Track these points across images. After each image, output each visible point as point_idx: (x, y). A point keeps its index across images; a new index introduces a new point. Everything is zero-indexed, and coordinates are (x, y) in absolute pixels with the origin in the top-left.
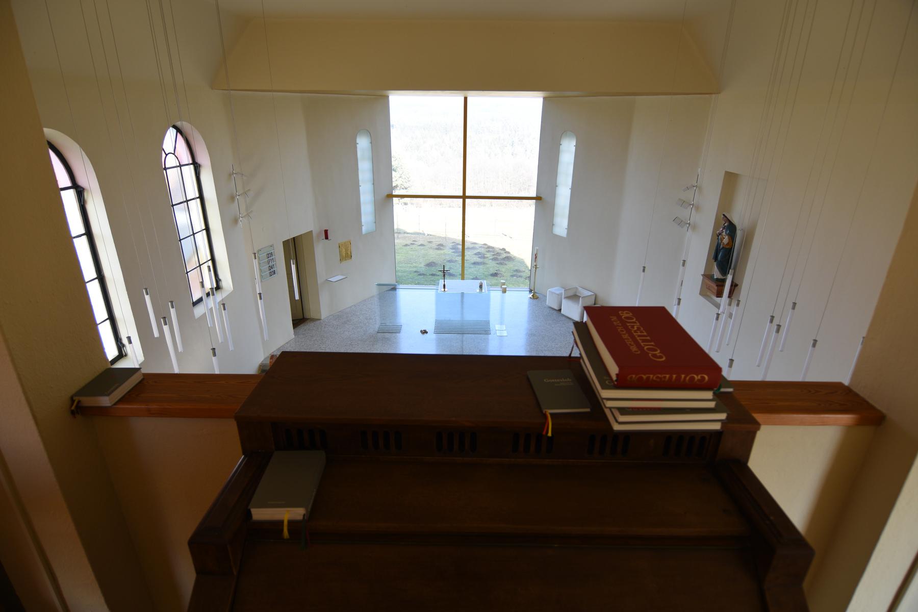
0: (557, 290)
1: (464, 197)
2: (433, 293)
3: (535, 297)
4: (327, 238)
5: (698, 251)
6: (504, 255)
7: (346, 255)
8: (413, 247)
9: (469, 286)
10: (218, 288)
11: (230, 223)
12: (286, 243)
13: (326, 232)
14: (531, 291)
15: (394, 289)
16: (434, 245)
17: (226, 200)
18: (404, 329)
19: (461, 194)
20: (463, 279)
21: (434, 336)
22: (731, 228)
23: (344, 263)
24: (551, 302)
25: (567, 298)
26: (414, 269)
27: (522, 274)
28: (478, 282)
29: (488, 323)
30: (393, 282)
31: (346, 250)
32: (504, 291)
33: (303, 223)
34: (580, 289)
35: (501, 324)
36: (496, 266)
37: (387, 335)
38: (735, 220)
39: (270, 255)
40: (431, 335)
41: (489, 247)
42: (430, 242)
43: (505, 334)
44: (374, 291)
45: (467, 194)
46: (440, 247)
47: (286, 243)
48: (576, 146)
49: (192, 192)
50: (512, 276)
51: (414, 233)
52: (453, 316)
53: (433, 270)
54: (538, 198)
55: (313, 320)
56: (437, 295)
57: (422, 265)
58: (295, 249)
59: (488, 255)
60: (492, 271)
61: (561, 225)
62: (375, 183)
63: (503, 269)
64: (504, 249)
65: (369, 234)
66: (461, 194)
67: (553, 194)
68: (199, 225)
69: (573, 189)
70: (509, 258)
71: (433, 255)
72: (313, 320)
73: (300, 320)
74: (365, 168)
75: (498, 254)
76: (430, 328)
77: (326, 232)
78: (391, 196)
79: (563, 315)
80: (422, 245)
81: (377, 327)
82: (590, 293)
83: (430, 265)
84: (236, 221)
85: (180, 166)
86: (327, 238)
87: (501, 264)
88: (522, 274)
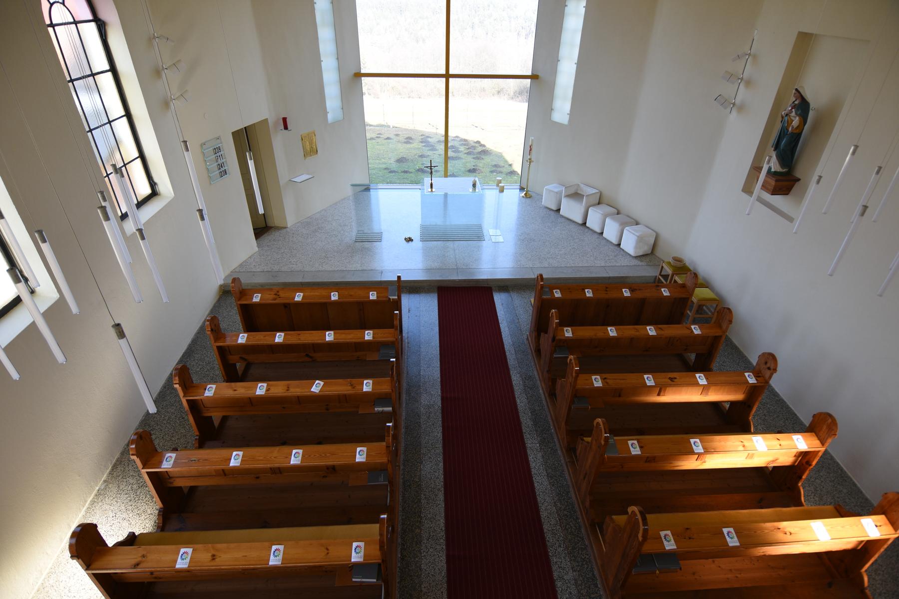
0: (554, 187)
1: (447, 76)
2: (418, 193)
3: (527, 196)
4: (286, 128)
5: (743, 137)
6: (480, 149)
7: (311, 151)
8: (379, 140)
9: (459, 186)
10: (154, 194)
11: (159, 107)
12: (236, 135)
13: (285, 120)
14: (522, 189)
15: (368, 189)
16: (401, 139)
17: (149, 75)
18: (385, 236)
19: (444, 72)
20: (446, 176)
21: (420, 244)
22: (803, 106)
23: (308, 158)
24: (548, 201)
25: (567, 196)
26: (384, 166)
27: (501, 169)
28: (470, 180)
29: (480, 227)
30: (366, 182)
31: (311, 143)
32: (502, 191)
33: (256, 109)
34: (582, 186)
35: (496, 227)
36: (478, 161)
37: (366, 245)
38: (809, 96)
39: (217, 150)
40: (417, 243)
41: (462, 140)
42: (397, 135)
43: (501, 239)
44: (349, 191)
45: (443, 71)
46: (409, 140)
47: (236, 135)
48: (586, 7)
49: (100, 62)
50: (492, 172)
51: (377, 126)
52: (436, 220)
53: (405, 166)
54: (534, 77)
55: (278, 228)
56: (423, 196)
57: (392, 161)
58: (247, 140)
59: (462, 149)
60: (470, 166)
61: (562, 109)
62: (339, 57)
63: (480, 164)
64: (478, 142)
65: (336, 123)
66: (444, 72)
67: (554, 72)
68: (117, 110)
69: (579, 64)
70: (485, 152)
71: (403, 150)
72: (278, 228)
73: (262, 228)
75: (474, 147)
76: (416, 235)
77: (285, 120)
78: (359, 75)
79: (562, 216)
80: (388, 138)
81: (354, 234)
82: (594, 191)
83: (401, 160)
84: (166, 104)
85: (76, 23)
86: (286, 128)
87: (478, 158)
88: (501, 169)
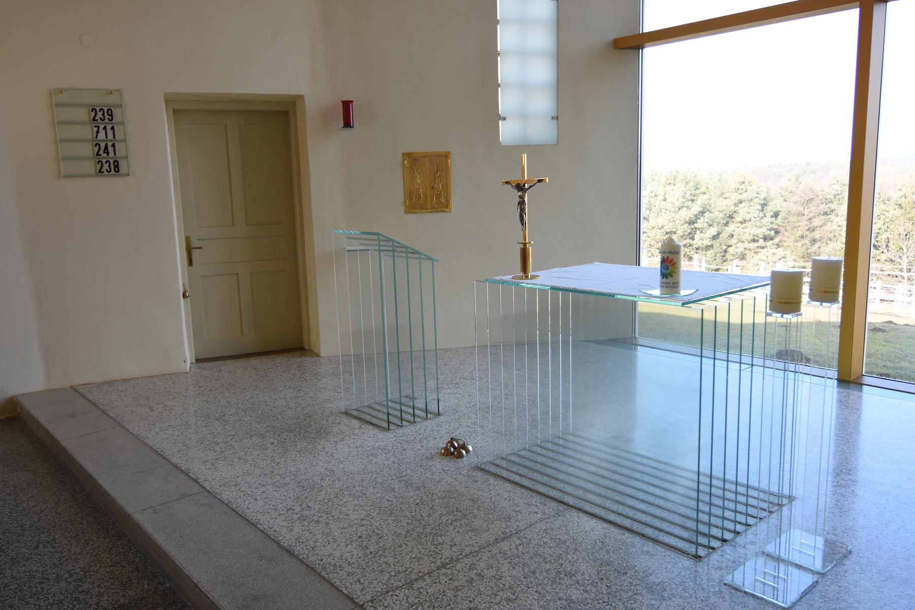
4: (347, 124)
13: (347, 105)
86: (347, 124)
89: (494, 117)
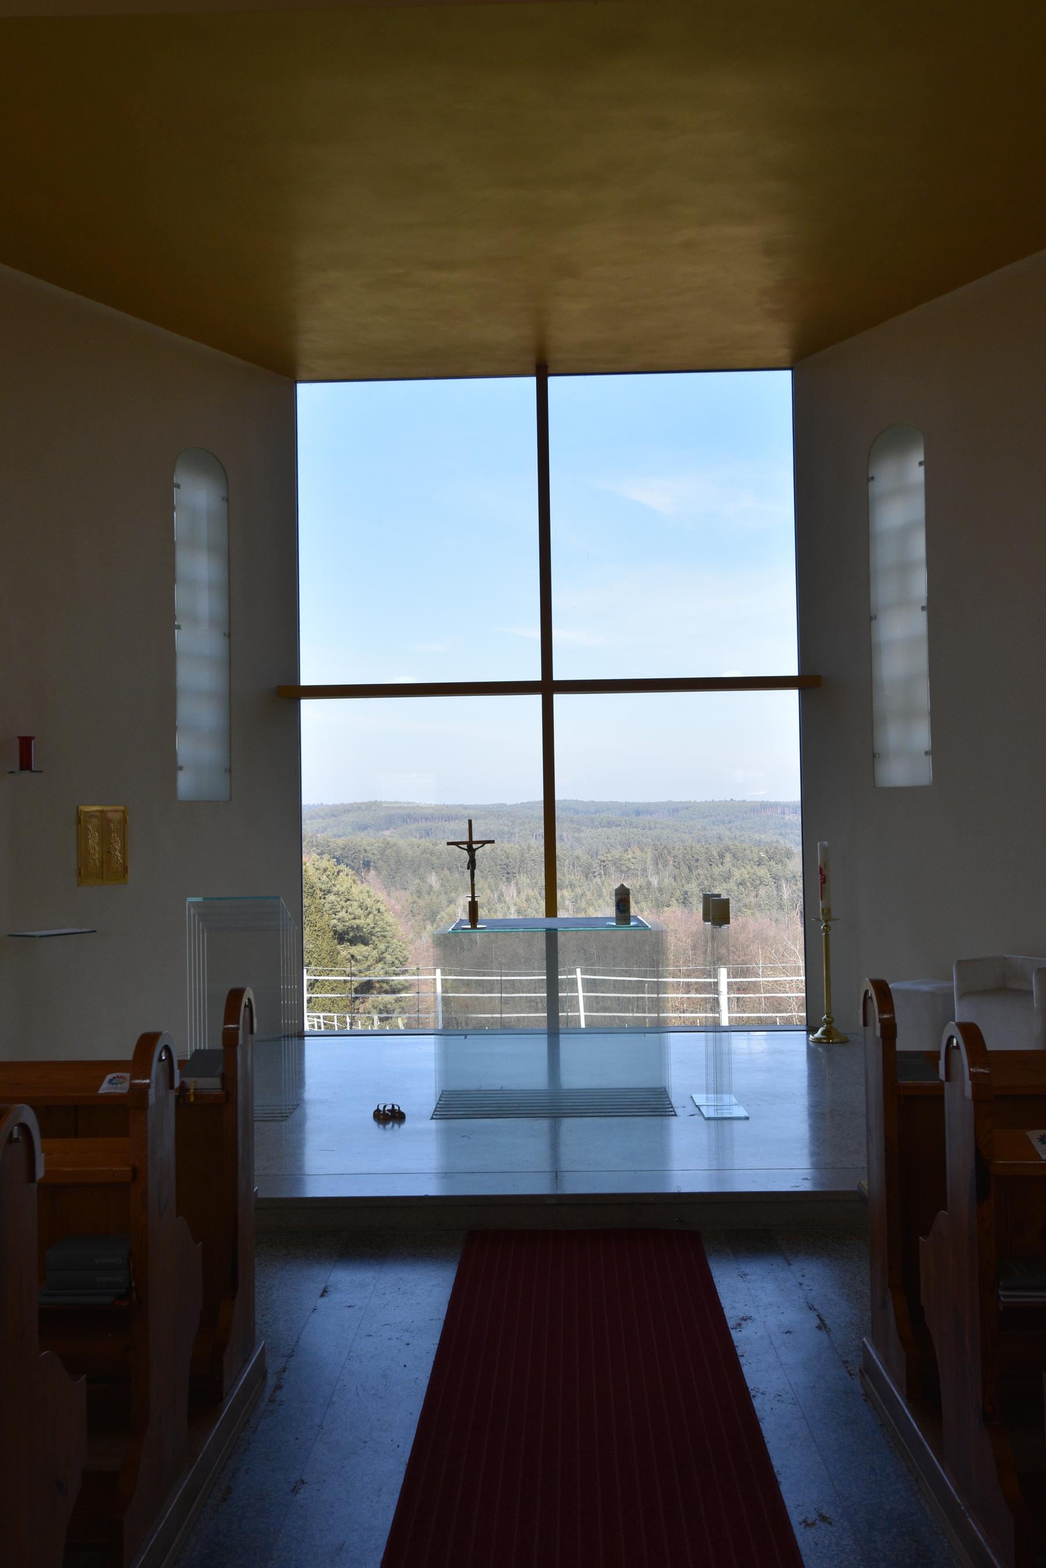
4: (25, 764)
13: (25, 743)
74: (198, 580)
86: (25, 764)
89: (171, 766)
